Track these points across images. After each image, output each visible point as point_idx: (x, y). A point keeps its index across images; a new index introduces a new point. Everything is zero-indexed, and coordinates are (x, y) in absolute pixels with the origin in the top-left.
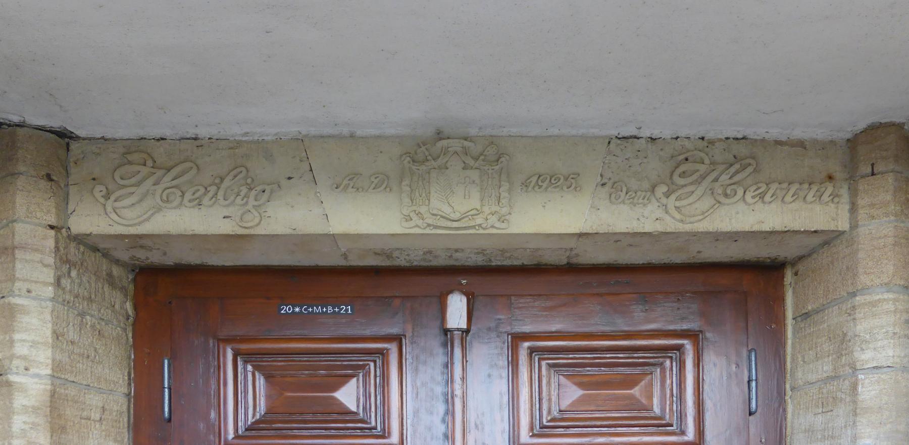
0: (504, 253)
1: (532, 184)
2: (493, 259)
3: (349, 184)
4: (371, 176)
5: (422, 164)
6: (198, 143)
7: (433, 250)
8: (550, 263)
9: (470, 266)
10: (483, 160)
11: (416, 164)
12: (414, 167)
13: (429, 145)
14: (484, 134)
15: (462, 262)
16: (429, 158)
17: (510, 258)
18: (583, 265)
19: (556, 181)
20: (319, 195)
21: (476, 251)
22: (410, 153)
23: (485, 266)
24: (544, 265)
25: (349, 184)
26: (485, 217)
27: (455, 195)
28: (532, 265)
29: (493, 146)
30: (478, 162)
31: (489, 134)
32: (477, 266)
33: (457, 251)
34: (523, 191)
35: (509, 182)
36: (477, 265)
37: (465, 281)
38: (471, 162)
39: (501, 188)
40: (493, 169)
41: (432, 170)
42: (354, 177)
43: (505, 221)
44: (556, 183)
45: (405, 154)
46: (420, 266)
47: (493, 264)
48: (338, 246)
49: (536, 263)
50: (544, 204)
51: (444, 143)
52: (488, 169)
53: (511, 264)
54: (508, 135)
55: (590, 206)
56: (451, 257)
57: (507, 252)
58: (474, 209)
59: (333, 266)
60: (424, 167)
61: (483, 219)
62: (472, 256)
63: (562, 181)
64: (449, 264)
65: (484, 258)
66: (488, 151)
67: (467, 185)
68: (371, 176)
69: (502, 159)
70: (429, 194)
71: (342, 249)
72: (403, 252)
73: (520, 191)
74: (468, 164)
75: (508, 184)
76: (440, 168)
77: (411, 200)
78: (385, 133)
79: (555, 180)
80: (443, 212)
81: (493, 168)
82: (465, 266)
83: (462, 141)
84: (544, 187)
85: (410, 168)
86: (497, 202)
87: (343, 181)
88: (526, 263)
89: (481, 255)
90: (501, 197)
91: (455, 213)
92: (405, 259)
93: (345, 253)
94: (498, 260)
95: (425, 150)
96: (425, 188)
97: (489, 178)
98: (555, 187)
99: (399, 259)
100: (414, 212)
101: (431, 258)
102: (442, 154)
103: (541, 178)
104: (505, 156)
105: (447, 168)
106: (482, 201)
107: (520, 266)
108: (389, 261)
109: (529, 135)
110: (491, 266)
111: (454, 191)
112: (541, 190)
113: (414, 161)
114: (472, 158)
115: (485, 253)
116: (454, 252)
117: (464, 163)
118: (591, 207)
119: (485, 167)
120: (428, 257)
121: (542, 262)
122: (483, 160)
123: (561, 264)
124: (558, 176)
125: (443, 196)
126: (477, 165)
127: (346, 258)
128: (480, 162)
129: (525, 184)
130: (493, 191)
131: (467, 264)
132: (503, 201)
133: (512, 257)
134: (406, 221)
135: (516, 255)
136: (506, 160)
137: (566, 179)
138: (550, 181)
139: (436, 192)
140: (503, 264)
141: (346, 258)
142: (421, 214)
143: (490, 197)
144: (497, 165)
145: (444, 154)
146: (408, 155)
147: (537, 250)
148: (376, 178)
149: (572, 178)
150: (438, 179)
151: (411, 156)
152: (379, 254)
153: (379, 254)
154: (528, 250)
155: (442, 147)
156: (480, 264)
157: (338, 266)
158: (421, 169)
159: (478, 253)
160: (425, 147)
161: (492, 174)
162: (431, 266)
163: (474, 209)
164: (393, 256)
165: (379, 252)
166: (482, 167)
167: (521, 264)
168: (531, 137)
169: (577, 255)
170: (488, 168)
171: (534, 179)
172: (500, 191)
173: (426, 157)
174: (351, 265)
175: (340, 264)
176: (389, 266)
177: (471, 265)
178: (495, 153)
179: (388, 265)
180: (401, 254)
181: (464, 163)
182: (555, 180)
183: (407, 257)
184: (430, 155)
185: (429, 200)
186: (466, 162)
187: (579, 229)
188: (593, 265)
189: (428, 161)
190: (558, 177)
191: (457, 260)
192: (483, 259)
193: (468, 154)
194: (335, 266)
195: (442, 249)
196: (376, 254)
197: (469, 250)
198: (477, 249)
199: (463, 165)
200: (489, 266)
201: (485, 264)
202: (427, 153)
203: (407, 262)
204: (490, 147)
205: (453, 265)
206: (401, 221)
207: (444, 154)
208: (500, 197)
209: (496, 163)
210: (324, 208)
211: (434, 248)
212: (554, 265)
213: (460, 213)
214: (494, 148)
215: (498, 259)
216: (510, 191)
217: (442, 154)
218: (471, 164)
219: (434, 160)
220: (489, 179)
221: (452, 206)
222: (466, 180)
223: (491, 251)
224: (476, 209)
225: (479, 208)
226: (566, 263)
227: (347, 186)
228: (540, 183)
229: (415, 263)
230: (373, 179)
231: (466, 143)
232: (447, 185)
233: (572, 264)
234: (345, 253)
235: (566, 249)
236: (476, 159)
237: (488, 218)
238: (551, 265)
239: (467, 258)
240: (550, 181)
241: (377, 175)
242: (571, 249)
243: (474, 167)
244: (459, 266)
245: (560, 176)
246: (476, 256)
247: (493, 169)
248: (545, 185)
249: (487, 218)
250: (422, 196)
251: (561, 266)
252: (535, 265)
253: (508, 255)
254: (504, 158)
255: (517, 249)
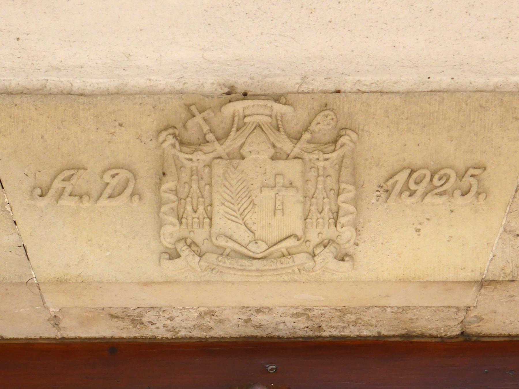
0: (345, 315)
1: (398, 187)
2: (324, 325)
3: (64, 188)
4: (104, 172)
5: (196, 150)
6: (249, 309)
7: (217, 309)
8: (430, 332)
9: (283, 338)
10: (309, 142)
11: (185, 149)
12: (182, 156)
13: (208, 111)
14: (311, 87)
15: (269, 331)
16: (210, 137)
17: (355, 323)
18: (490, 336)
19: (442, 182)
20: (9, 209)
21: (295, 311)
22: (175, 127)
23: (309, 337)
24: (418, 336)
25: (64, 188)
26: (310, 250)
27: (256, 209)
28: (394, 336)
29: (327, 112)
30: (298, 145)
31: (321, 88)
32: (294, 338)
33: (259, 311)
34: (380, 200)
35: (354, 184)
36: (296, 336)
37: (274, 367)
38: (287, 146)
39: (340, 197)
40: (326, 160)
41: (217, 161)
42: (73, 175)
43: (347, 259)
44: (442, 185)
45: (166, 129)
46: (191, 338)
47: (326, 334)
48: (44, 303)
49: (403, 332)
50: (419, 227)
51: (239, 106)
52: (318, 159)
53: (357, 334)
54: (354, 90)
55: (502, 229)
56: (248, 321)
57: (350, 312)
58: (291, 236)
59: (31, 339)
60: (199, 156)
61: (306, 255)
62: (287, 319)
63: (452, 180)
64: (243, 335)
65: (310, 324)
66: (318, 123)
67: (279, 191)
68: (104, 172)
69: (343, 140)
70: (209, 208)
71: (51, 310)
72: (161, 313)
73: (374, 201)
74: (281, 149)
75: (351, 187)
76: (230, 157)
77: (178, 219)
78: (126, 85)
79: (440, 179)
80: (235, 241)
81: (327, 156)
82: (273, 337)
83: (270, 103)
84: (419, 193)
85: (176, 158)
86: (332, 221)
87: (52, 181)
88: (384, 332)
89: (304, 318)
90: (341, 213)
91: (256, 243)
92: (165, 326)
93: (55, 316)
94: (334, 328)
95: (201, 122)
96: (203, 197)
97: (318, 176)
98: (440, 194)
99: (154, 326)
100: (183, 241)
101: (212, 324)
102: (234, 129)
103: (415, 175)
104: (348, 132)
105: (243, 158)
106: (305, 220)
107: (374, 337)
108: (134, 330)
109: (394, 89)
110: (320, 337)
111: (256, 202)
112: (414, 199)
113: (181, 143)
114: (289, 136)
115: (311, 314)
116: (255, 313)
117: (274, 146)
118: (505, 230)
119: (311, 156)
120: (208, 321)
121: (414, 332)
122: (309, 142)
123: (449, 334)
124: (442, 172)
125: (235, 211)
126: (297, 151)
127: (56, 325)
128: (302, 144)
129: (385, 187)
130: (326, 200)
131: (276, 334)
132: (343, 220)
133: (360, 321)
134: (170, 259)
135: (366, 319)
136: (351, 141)
137: (461, 177)
138: (431, 180)
139: (223, 204)
140: (342, 334)
141: (56, 325)
142: (197, 245)
143: (321, 213)
144: (334, 151)
145: (238, 130)
146: (171, 131)
147: (405, 309)
148: (113, 176)
149: (472, 176)
150: (226, 179)
151: (177, 134)
152: (117, 317)
153: (117, 317)
154: (389, 310)
155: (234, 117)
156: (302, 333)
157: (41, 338)
158: (194, 159)
159: (297, 315)
160: (201, 115)
161: (324, 168)
162: (211, 338)
163: (291, 236)
164: (145, 320)
165: (119, 314)
166: (307, 156)
167: (377, 335)
168: (398, 92)
169: (480, 319)
170: (316, 157)
171: (402, 177)
172: (339, 203)
173: (205, 135)
174: (65, 336)
175: (46, 335)
176: (135, 338)
177: (285, 336)
178: (330, 127)
179: (132, 335)
180: (159, 316)
181: (274, 146)
182: (440, 179)
183: (168, 322)
184: (211, 132)
185: (211, 219)
186: (278, 145)
187: (482, 274)
188: (509, 336)
189: (208, 142)
190: (445, 175)
191: (259, 327)
192: (306, 325)
193: (281, 129)
194: (35, 339)
195: (233, 308)
196: (112, 316)
197: (282, 310)
198: (297, 308)
199: (272, 151)
200: (318, 337)
201: (310, 333)
202: (206, 128)
203: (169, 331)
204: (322, 114)
205: (252, 337)
206: (160, 258)
207: (238, 130)
208: (337, 213)
209: (332, 148)
210: (19, 235)
211: (218, 307)
212: (437, 337)
213: (267, 244)
214: (330, 117)
215: (333, 324)
216: (356, 202)
217: (234, 129)
218: (285, 149)
219: (218, 140)
220: (319, 179)
221: (252, 229)
222: (277, 180)
223: (320, 312)
224: (295, 236)
225: (300, 233)
226: (458, 333)
227: (61, 194)
228: (413, 187)
229: (183, 333)
230: (107, 178)
231: (278, 108)
232: (243, 190)
233: (469, 335)
234: (55, 316)
235: (458, 309)
236: (296, 139)
237: (316, 253)
238: (431, 336)
239: (278, 324)
240: (431, 180)
241: (115, 171)
242: (468, 309)
243: (292, 155)
244: (262, 337)
245: (448, 171)
246: (294, 320)
247: (326, 160)
248: (421, 188)
249: (314, 253)
250: (198, 211)
251: (450, 337)
252: (402, 336)
253: (353, 317)
254: (347, 137)
255: (368, 308)
